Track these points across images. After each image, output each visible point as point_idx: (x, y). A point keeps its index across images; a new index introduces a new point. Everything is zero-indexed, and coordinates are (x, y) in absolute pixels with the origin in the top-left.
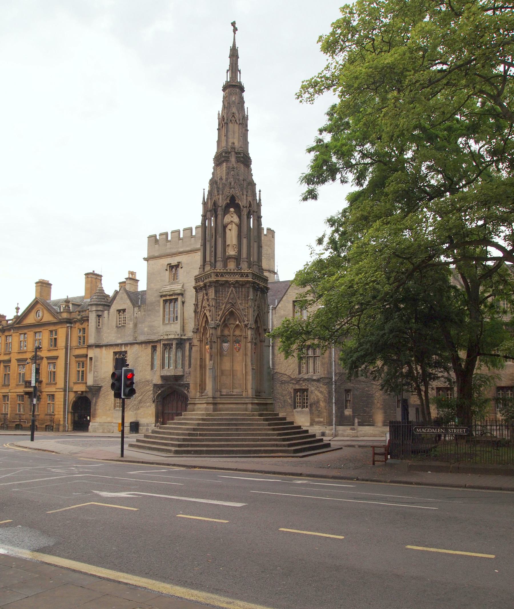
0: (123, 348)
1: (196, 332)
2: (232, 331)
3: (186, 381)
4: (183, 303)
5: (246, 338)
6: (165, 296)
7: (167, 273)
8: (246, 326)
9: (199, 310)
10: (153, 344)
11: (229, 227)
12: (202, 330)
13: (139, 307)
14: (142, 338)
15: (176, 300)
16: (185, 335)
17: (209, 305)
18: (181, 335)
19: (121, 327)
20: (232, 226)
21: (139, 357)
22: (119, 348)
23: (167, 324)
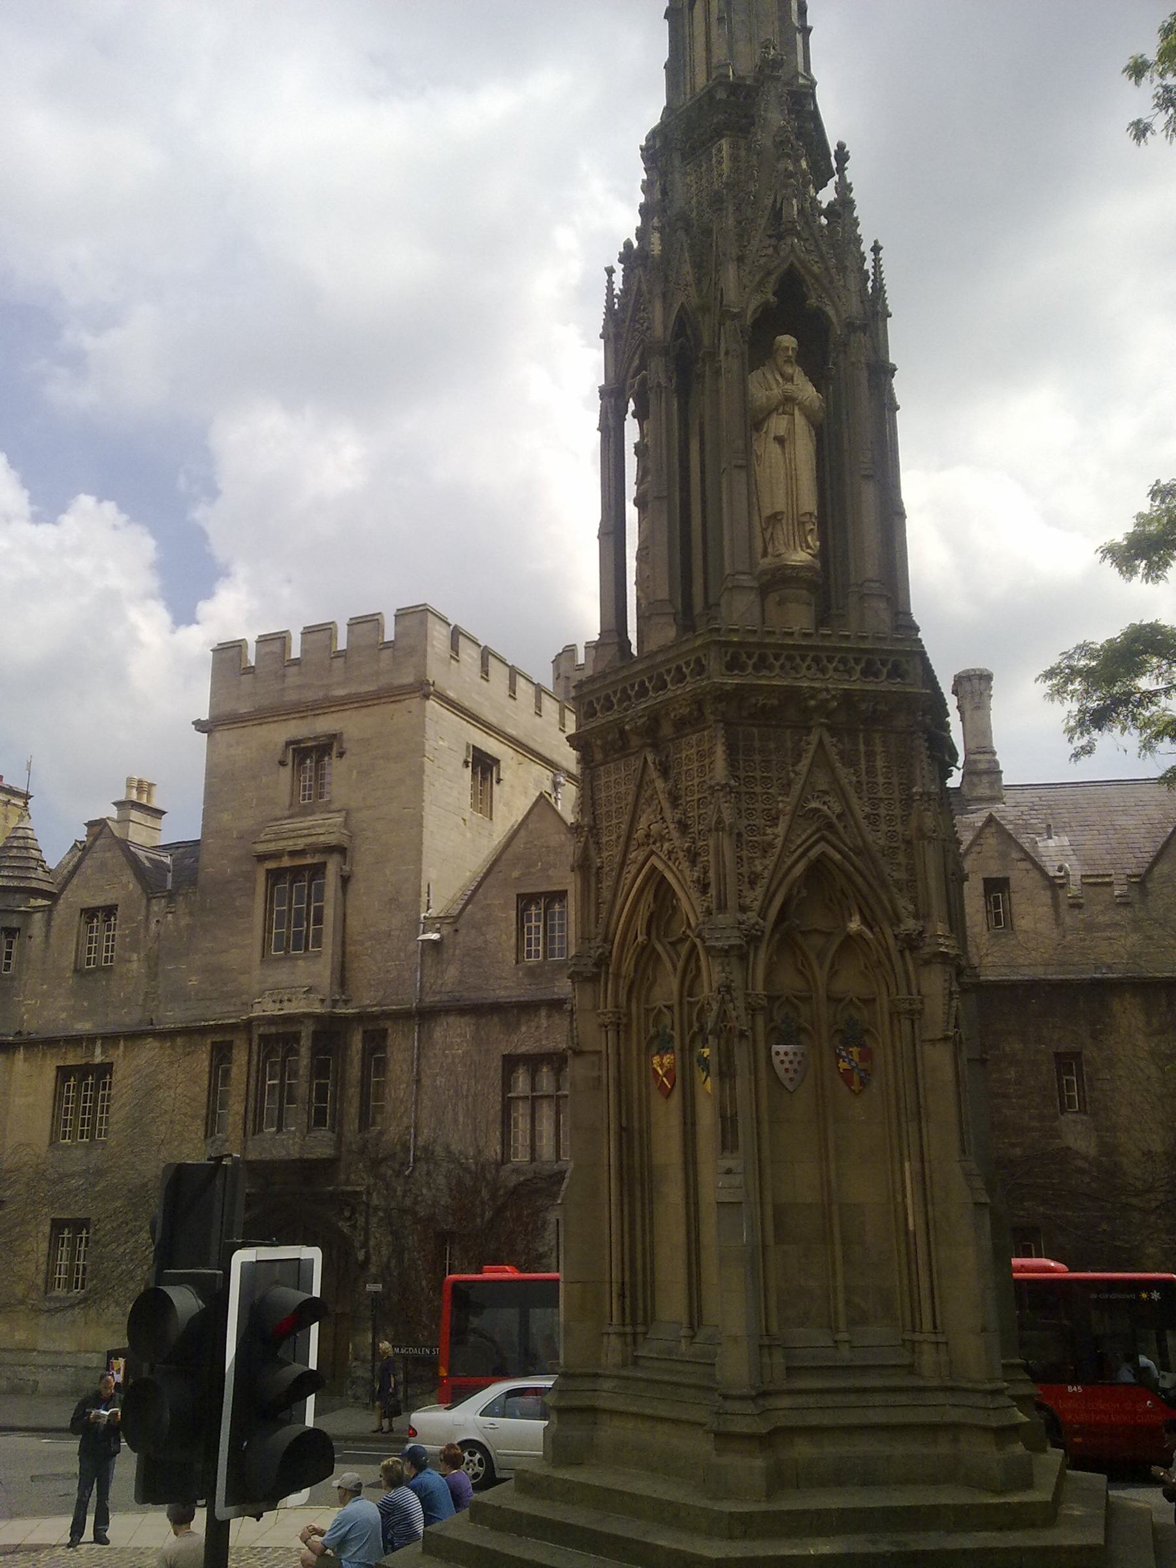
0: (98, 1051)
1: (594, 979)
2: (821, 976)
3: (348, 1182)
4: (345, 880)
5: (915, 1015)
6: (275, 856)
7: (286, 773)
8: (911, 944)
9: (610, 855)
10: (220, 1042)
11: (778, 425)
12: (628, 966)
13: (171, 897)
14: (172, 1016)
15: (318, 870)
16: (346, 1002)
17: (683, 827)
18: (335, 1003)
19: (90, 973)
20: (792, 422)
21: (159, 1087)
22: (80, 1052)
23: (280, 959)
